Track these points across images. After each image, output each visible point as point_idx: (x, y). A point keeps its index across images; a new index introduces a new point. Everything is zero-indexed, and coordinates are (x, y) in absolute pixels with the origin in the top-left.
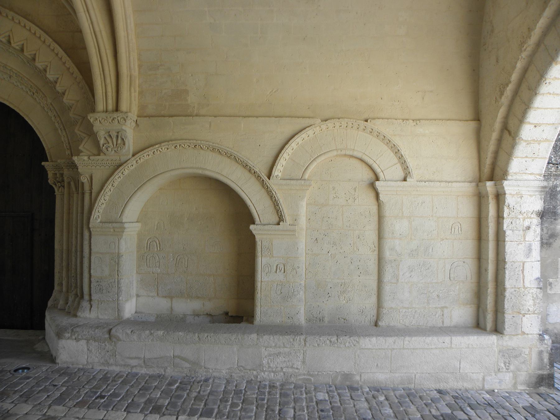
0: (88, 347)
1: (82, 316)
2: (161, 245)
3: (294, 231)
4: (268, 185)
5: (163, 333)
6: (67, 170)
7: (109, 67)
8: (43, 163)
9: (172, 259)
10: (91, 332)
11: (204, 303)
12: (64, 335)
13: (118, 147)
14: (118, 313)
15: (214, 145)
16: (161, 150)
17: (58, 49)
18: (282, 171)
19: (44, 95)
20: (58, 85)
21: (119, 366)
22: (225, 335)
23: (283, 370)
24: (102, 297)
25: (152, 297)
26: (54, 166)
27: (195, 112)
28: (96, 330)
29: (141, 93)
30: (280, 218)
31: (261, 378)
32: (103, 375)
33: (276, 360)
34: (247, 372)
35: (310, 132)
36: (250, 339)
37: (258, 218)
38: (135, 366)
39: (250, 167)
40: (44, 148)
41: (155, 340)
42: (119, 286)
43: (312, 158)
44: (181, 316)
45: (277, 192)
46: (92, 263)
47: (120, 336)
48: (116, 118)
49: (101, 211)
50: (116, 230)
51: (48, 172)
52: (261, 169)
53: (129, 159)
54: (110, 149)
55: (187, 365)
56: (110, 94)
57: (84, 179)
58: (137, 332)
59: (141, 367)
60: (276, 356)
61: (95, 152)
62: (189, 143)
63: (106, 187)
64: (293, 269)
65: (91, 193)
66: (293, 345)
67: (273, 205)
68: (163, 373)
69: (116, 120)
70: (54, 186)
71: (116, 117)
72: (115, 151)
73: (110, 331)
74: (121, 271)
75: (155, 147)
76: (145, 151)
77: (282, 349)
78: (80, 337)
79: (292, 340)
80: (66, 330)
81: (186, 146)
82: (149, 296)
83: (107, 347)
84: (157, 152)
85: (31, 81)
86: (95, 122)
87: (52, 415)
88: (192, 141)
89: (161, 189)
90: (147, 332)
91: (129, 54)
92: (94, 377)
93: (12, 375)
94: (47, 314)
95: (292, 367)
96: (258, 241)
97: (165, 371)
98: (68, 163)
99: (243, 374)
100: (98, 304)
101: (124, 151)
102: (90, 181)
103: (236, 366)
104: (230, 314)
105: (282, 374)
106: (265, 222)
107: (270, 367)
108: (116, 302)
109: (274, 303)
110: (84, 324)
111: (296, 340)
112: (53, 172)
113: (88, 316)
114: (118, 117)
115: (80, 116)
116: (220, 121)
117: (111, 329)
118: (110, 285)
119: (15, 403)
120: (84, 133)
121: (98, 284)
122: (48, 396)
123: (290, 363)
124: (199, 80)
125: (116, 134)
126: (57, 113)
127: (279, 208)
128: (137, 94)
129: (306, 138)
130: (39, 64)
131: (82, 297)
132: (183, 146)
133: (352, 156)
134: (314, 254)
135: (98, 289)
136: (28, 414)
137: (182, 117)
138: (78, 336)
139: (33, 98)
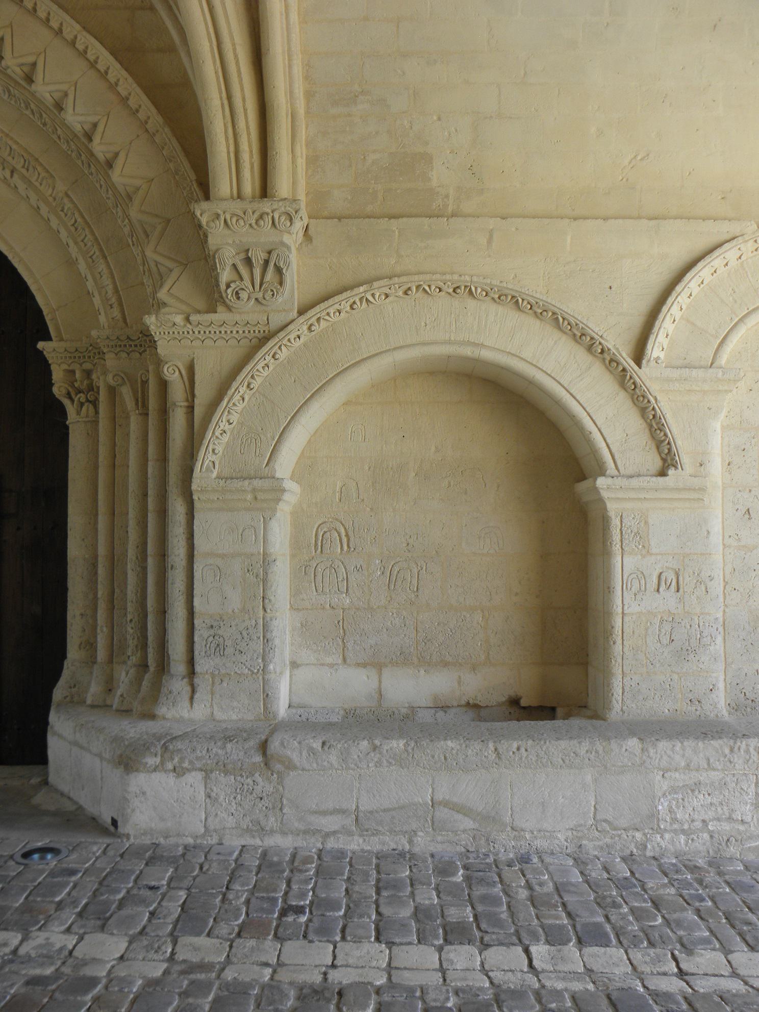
1: (169, 716)
2: (352, 539)
3: (702, 490)
4: (638, 380)
5: (405, 745)
6: (113, 355)
7: (242, 90)
8: (41, 345)
9: (379, 573)
10: (214, 750)
11: (460, 677)
12: (144, 761)
13: (266, 291)
14: (264, 704)
17: (97, 50)
18: (665, 347)
19: (47, 171)
20: (97, 139)
21: (292, 833)
22: (563, 744)
23: (707, 826)
24: (224, 665)
25: (331, 666)
26: (70, 353)
28: (229, 746)
29: (313, 161)
30: (664, 460)
31: (653, 847)
32: (258, 859)
33: (689, 802)
34: (619, 836)
35: (730, 253)
36: (626, 750)
37: (611, 461)
38: (334, 833)
39: (592, 338)
40: (40, 311)
41: (385, 761)
42: (268, 636)
43: (737, 316)
44: (404, 711)
45: (658, 398)
46: (195, 582)
47: (295, 757)
48: (268, 214)
49: (220, 449)
50: (260, 496)
51: (53, 367)
53: (292, 321)
54: (244, 295)
55: (469, 824)
56: (245, 157)
57: (173, 375)
58: (339, 746)
59: (350, 834)
60: (689, 792)
61: (201, 304)
63: (233, 390)
65: (191, 408)
66: (730, 762)
67: (647, 431)
68: (407, 847)
70: (66, 402)
71: (269, 211)
72: (256, 299)
73: (264, 747)
74: (272, 598)
75: (356, 291)
76: (331, 301)
77: (704, 774)
78: (186, 765)
79: (727, 751)
80: (148, 748)
81: (433, 288)
82: (323, 665)
83: (258, 789)
84: (361, 306)
85: (12, 139)
86: (212, 224)
87: (194, 960)
89: (347, 403)
90: (365, 744)
91: (290, 60)
92: (239, 865)
93: (22, 867)
94: (53, 717)
95: (730, 819)
96: (613, 517)
97: (410, 842)
99: (608, 840)
100: (213, 683)
101: (280, 300)
102: (185, 378)
103: (591, 822)
104: (523, 703)
105: (706, 836)
106: (629, 471)
107: (676, 819)
108: (261, 678)
110: (184, 734)
111: (739, 749)
112: (65, 367)
113: (185, 714)
115: (157, 216)
116: (517, 229)
117: (266, 741)
119: (76, 933)
120: (169, 258)
121: (212, 632)
122: (152, 914)
123: (725, 808)
124: (456, 131)
125: (264, 256)
126: (83, 217)
127: (666, 435)
128: (304, 161)
129: (722, 270)
130: (44, 90)
132: (427, 288)
134: (743, 546)
136: (127, 960)
137: (423, 219)
138: (179, 763)
139: (9, 185)
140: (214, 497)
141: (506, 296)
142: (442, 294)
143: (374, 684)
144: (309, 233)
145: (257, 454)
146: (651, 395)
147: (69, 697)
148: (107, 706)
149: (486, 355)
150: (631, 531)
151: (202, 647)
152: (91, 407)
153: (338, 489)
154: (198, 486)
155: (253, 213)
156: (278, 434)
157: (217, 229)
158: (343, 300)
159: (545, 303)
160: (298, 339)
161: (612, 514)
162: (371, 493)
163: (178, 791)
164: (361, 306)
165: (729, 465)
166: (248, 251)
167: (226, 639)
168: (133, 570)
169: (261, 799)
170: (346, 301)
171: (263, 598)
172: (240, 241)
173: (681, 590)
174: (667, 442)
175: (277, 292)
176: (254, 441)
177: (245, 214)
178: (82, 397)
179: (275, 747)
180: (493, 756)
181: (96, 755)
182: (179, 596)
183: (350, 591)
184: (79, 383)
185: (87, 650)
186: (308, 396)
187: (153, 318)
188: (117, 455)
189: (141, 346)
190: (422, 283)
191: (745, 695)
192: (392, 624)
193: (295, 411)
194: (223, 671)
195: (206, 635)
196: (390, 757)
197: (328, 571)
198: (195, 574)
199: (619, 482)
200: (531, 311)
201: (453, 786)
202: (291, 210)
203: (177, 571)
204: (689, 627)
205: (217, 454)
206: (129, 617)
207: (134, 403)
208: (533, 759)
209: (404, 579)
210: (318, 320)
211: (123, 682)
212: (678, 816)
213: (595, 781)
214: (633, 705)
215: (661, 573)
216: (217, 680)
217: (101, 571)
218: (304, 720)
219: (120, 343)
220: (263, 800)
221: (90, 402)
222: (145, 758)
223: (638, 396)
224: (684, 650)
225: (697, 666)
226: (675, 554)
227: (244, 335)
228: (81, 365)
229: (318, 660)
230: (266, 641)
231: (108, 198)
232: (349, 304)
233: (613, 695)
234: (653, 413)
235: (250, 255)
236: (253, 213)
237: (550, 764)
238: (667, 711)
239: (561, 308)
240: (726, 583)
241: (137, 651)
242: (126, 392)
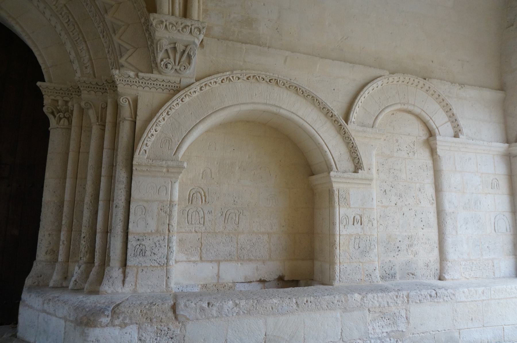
0: (140, 336)
1: (109, 292)
2: (207, 197)
8: (39, 84)
13: (181, 66)
16: (231, 78)
25: (194, 262)
35: (379, 82)
36: (354, 299)
39: (328, 110)
41: (242, 312)
44: (230, 284)
48: (188, 26)
49: (149, 144)
50: (171, 170)
52: (338, 112)
54: (170, 66)
58: (217, 304)
60: (381, 318)
62: (265, 75)
63: (160, 114)
64: (369, 222)
66: (397, 303)
69: (188, 29)
70: (50, 117)
71: (190, 25)
72: (176, 70)
75: (225, 74)
76: (213, 77)
80: (103, 312)
82: (189, 261)
94: (25, 296)
96: (335, 190)
98: (91, 83)
104: (286, 279)
108: (165, 268)
109: (353, 260)
111: (400, 297)
114: (191, 25)
118: (157, 244)
121: (139, 243)
125: (183, 48)
126: (74, 19)
131: (105, 262)
133: (410, 112)
135: (139, 251)
140: (144, 169)
141: (292, 86)
142: (264, 81)
143: (216, 271)
144: (203, 43)
145: (170, 148)
146: (352, 137)
147: (36, 283)
148: (63, 287)
149: (282, 112)
150: (343, 197)
151: (132, 251)
152: (66, 121)
153: (201, 172)
154: (137, 162)
155: (181, 24)
156: (181, 139)
157: (161, 29)
158: (218, 77)
159: (310, 92)
160: (194, 93)
161: (335, 189)
162: (218, 175)
163: (121, 338)
164: (226, 82)
165: (378, 170)
166: (175, 43)
167: (147, 246)
168: (88, 209)
169: (172, 338)
170: (220, 78)
171: (169, 224)
172: (173, 37)
173: (363, 224)
174: (358, 158)
175: (187, 68)
176: (168, 141)
177: (177, 24)
178: (62, 115)
179: (181, 307)
180: (295, 306)
181: (60, 318)
182: (120, 222)
183: (206, 223)
184: (60, 107)
185: (51, 255)
186: (198, 122)
188: (81, 147)
189: (103, 89)
190: (256, 75)
191: (386, 272)
192: (225, 241)
193: (191, 128)
195: (135, 244)
196: (244, 309)
197: (194, 213)
198: (131, 210)
199: (339, 174)
200: (302, 95)
201: (276, 323)
202: (201, 27)
203: (120, 209)
204: (366, 241)
205: (148, 146)
206: (83, 235)
207: (96, 119)
208: (314, 307)
209: (232, 218)
210: (206, 85)
211: (76, 273)
212: (377, 331)
213: (341, 316)
214: (344, 278)
215: (354, 217)
217: (66, 209)
218: (181, 291)
219: (91, 86)
220: (173, 339)
221: (66, 118)
222: (100, 318)
223: (346, 137)
224: (364, 251)
225: (369, 259)
226: (360, 208)
227: (166, 87)
228: (63, 97)
229: (187, 259)
230: (169, 247)
231: (90, 11)
232: (221, 79)
233: (335, 273)
234: (352, 145)
235: (176, 46)
236: (181, 24)
237: (321, 309)
238: (358, 280)
239: (316, 94)
240: (378, 222)
241: (87, 254)
242: (92, 114)
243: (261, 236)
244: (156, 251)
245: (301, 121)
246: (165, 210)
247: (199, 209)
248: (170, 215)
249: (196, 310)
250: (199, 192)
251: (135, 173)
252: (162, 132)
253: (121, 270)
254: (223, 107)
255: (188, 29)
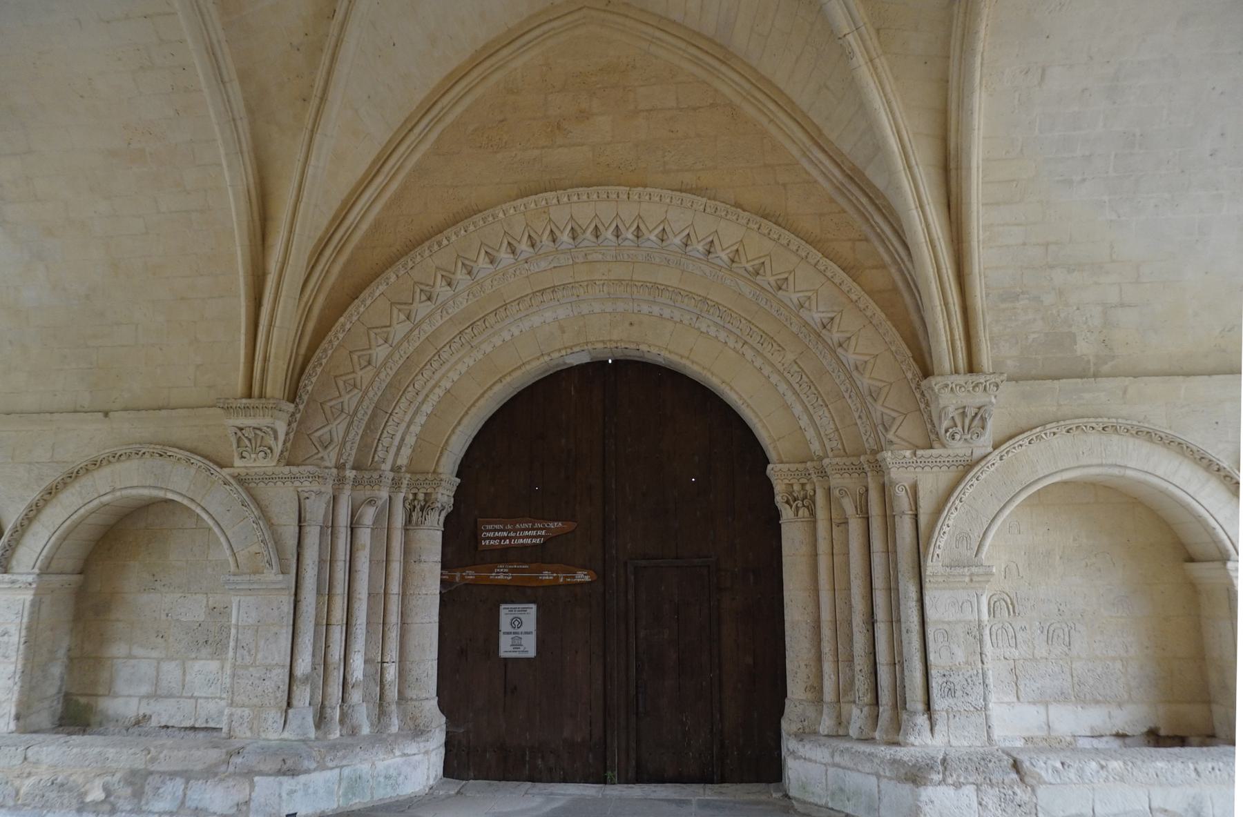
7: (953, 298)
11: (1110, 712)
15: (1141, 424)
16: (1044, 436)
25: (1009, 704)
27: (1092, 370)
41: (1112, 779)
44: (1068, 739)
47: (1043, 773)
48: (982, 383)
49: (942, 545)
50: (975, 578)
54: (957, 437)
65: (916, 516)
69: (981, 387)
71: (982, 381)
75: (1034, 431)
76: (1017, 439)
83: (1017, 799)
88: (1100, 420)
104: (1162, 732)
118: (969, 681)
121: (945, 680)
131: (899, 703)
135: (946, 690)
149: (1129, 473)
153: (1003, 569)
166: (964, 407)
180: (1193, 775)
183: (1019, 646)
187: (890, 453)
194: (955, 709)
197: (1000, 631)
216: (951, 716)
229: (998, 699)
243: (1111, 664)
244: (968, 690)
245: (1164, 485)
246: (973, 634)
247: (1007, 624)
248: (981, 641)
249: (1047, 770)
250: (1004, 600)
251: (927, 586)
252: (956, 526)
253: (926, 716)
254: (1036, 478)
255: (981, 387)
